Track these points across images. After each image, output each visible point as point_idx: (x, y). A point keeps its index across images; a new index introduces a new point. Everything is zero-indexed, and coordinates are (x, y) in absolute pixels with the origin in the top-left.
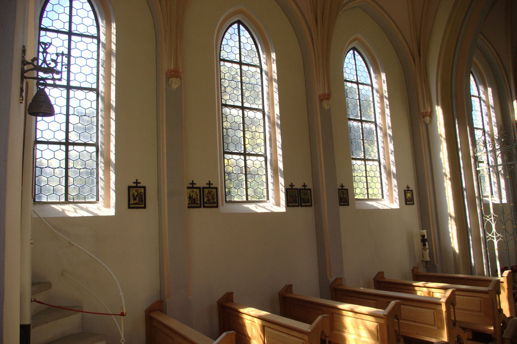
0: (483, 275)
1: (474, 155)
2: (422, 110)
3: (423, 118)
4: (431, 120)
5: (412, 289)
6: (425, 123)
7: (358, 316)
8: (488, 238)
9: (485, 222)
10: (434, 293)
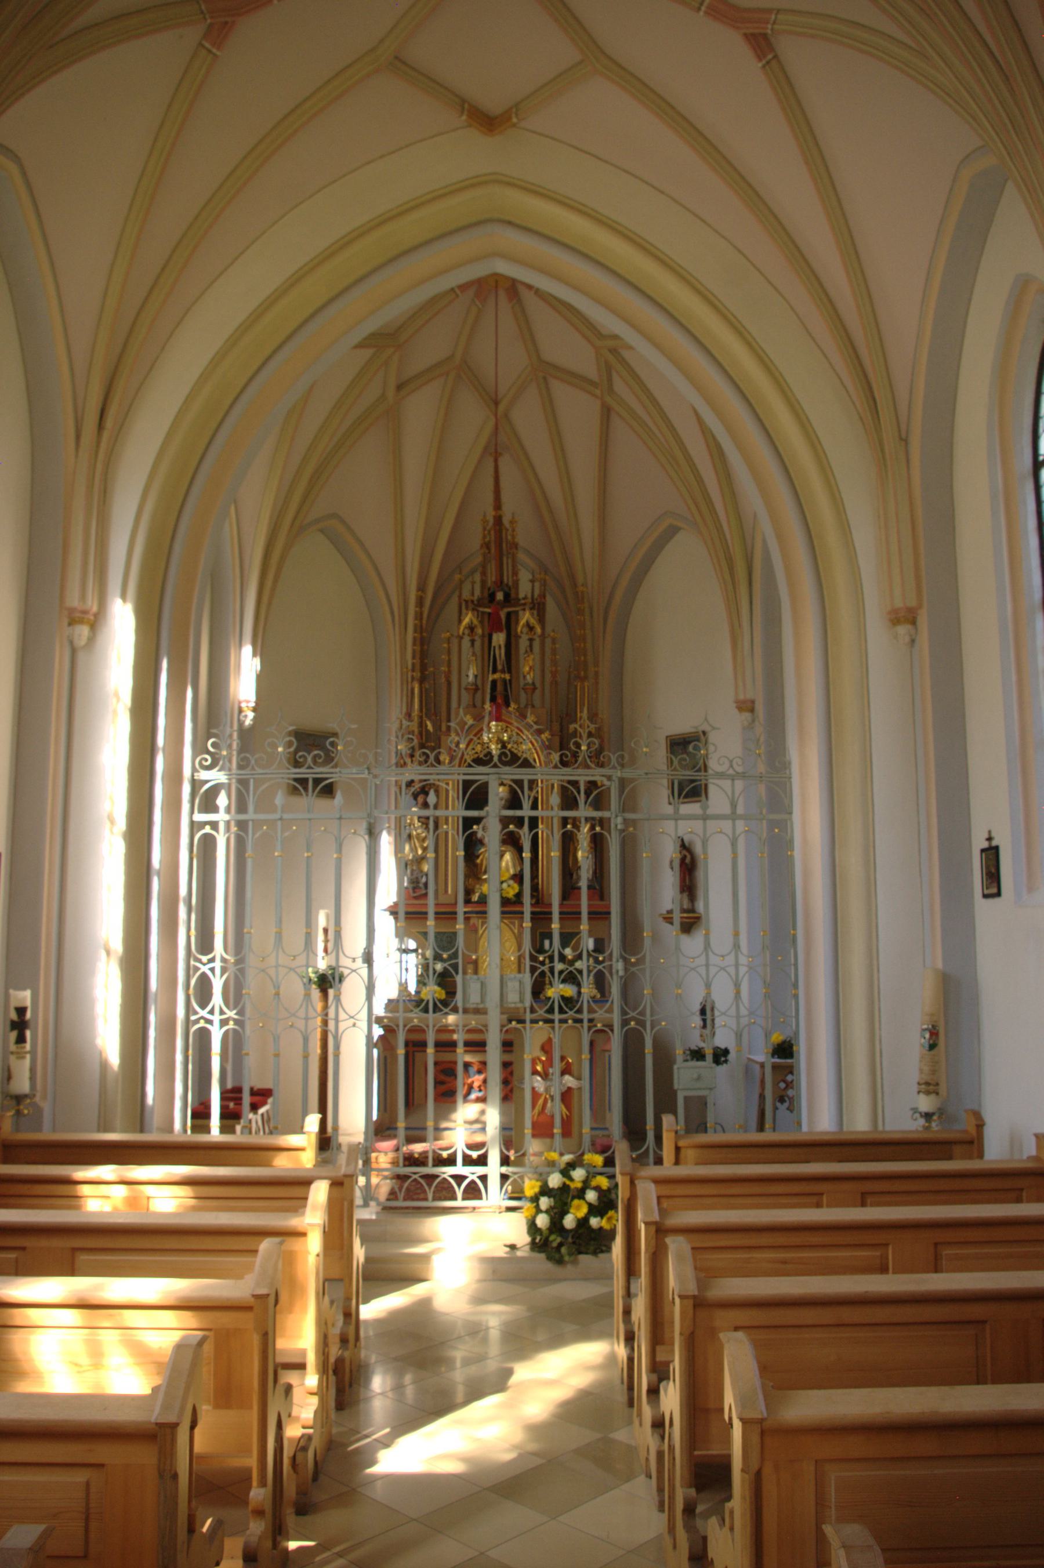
0: (170, 1129)
1: (193, 776)
2: (73, 600)
3: (70, 624)
4: (92, 640)
5: (70, 1194)
6: (71, 643)
7: (103, 1318)
8: (197, 1021)
9: (194, 974)
10: (151, 1200)
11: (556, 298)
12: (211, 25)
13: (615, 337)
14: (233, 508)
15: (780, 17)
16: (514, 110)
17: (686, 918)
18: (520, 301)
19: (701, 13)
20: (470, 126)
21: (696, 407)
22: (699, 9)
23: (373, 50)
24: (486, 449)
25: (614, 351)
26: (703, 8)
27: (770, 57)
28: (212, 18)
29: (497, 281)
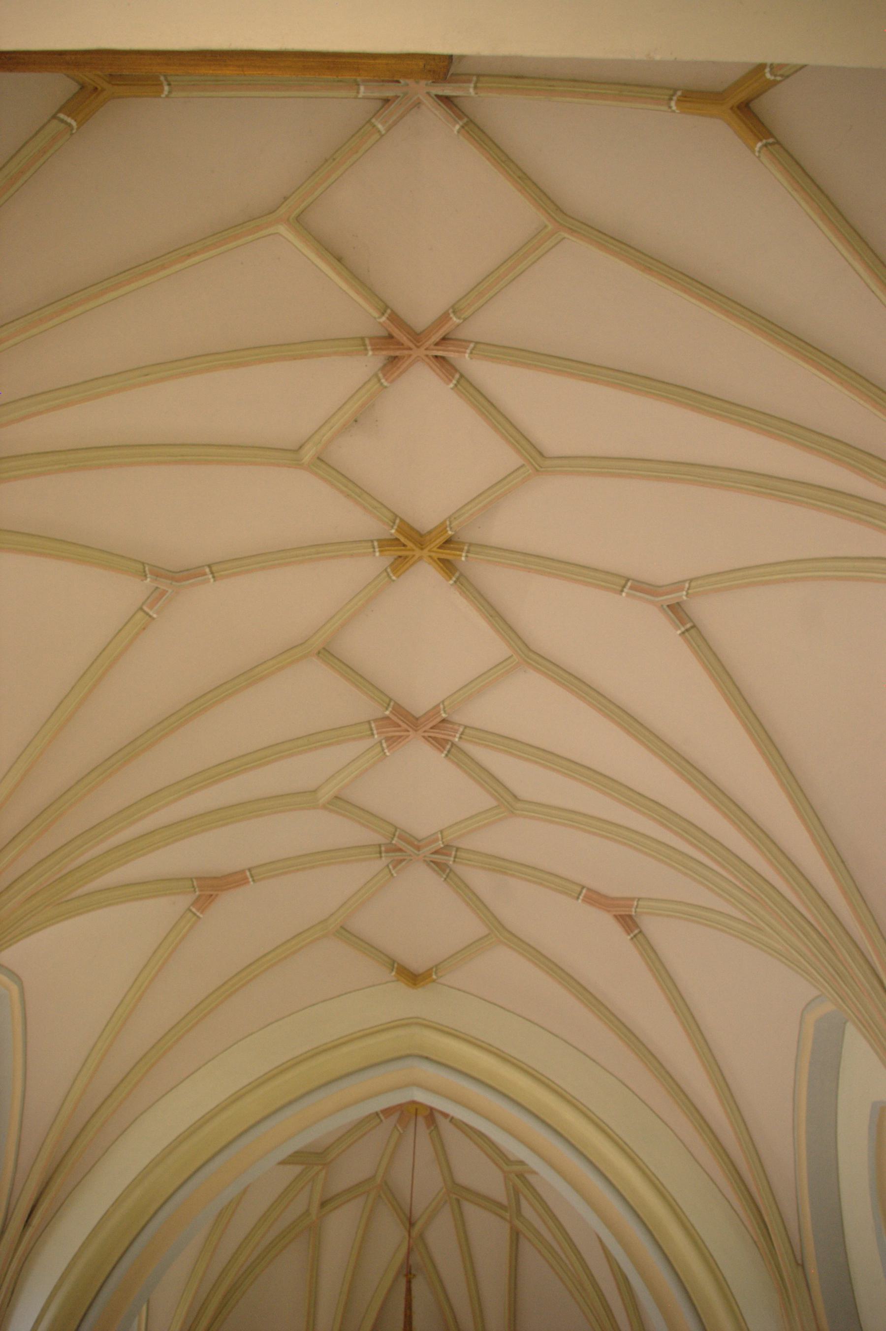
11: (467, 1125)
12: (200, 896)
13: (521, 1163)
14: (145, 1307)
15: (641, 903)
16: (434, 969)
17: (451, 735)
18: (436, 1127)
19: (580, 901)
20: (398, 980)
21: (601, 1235)
22: (578, 898)
23: (325, 920)
24: (398, 1273)
25: (521, 1176)
26: (581, 897)
27: (636, 931)
28: (201, 891)
29: (417, 1110)
